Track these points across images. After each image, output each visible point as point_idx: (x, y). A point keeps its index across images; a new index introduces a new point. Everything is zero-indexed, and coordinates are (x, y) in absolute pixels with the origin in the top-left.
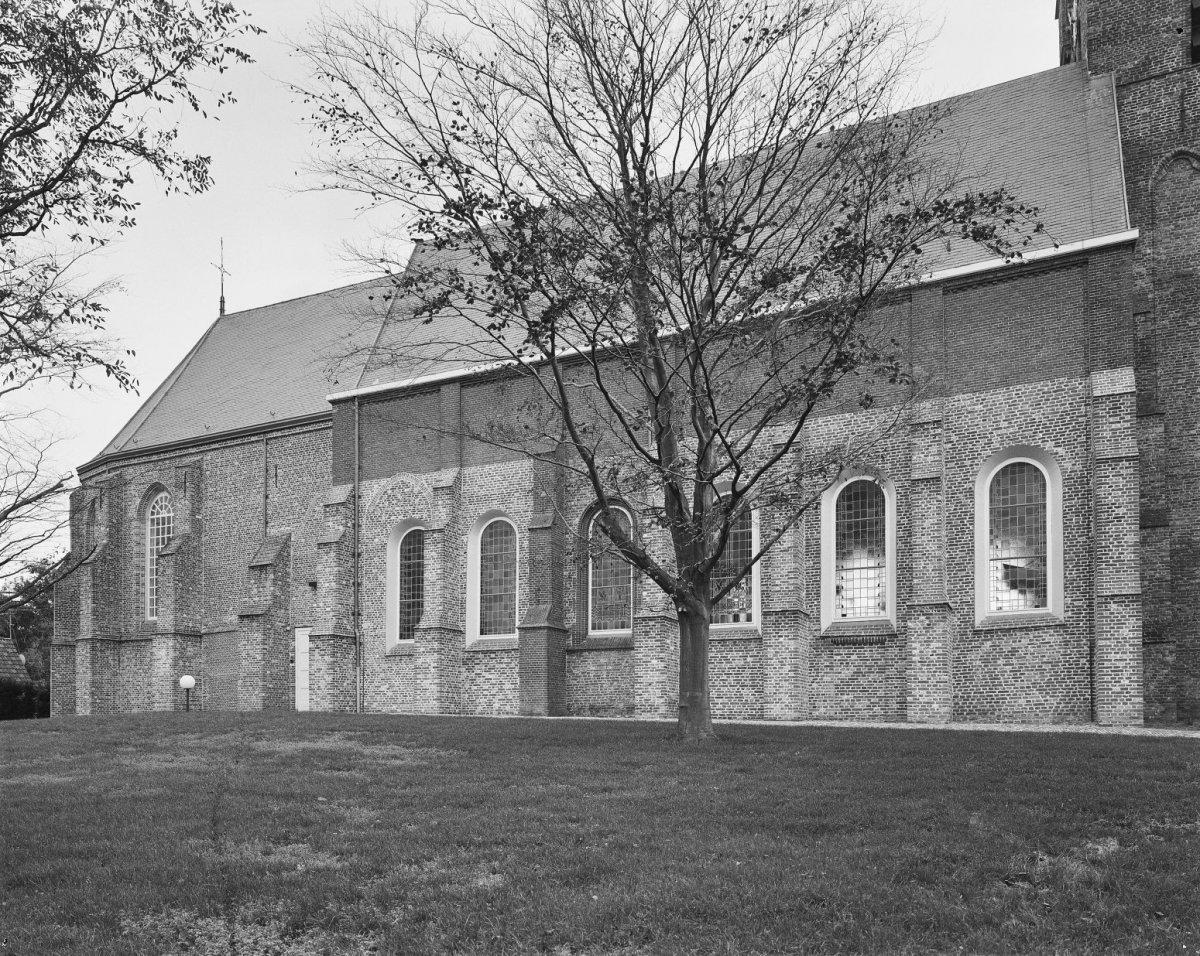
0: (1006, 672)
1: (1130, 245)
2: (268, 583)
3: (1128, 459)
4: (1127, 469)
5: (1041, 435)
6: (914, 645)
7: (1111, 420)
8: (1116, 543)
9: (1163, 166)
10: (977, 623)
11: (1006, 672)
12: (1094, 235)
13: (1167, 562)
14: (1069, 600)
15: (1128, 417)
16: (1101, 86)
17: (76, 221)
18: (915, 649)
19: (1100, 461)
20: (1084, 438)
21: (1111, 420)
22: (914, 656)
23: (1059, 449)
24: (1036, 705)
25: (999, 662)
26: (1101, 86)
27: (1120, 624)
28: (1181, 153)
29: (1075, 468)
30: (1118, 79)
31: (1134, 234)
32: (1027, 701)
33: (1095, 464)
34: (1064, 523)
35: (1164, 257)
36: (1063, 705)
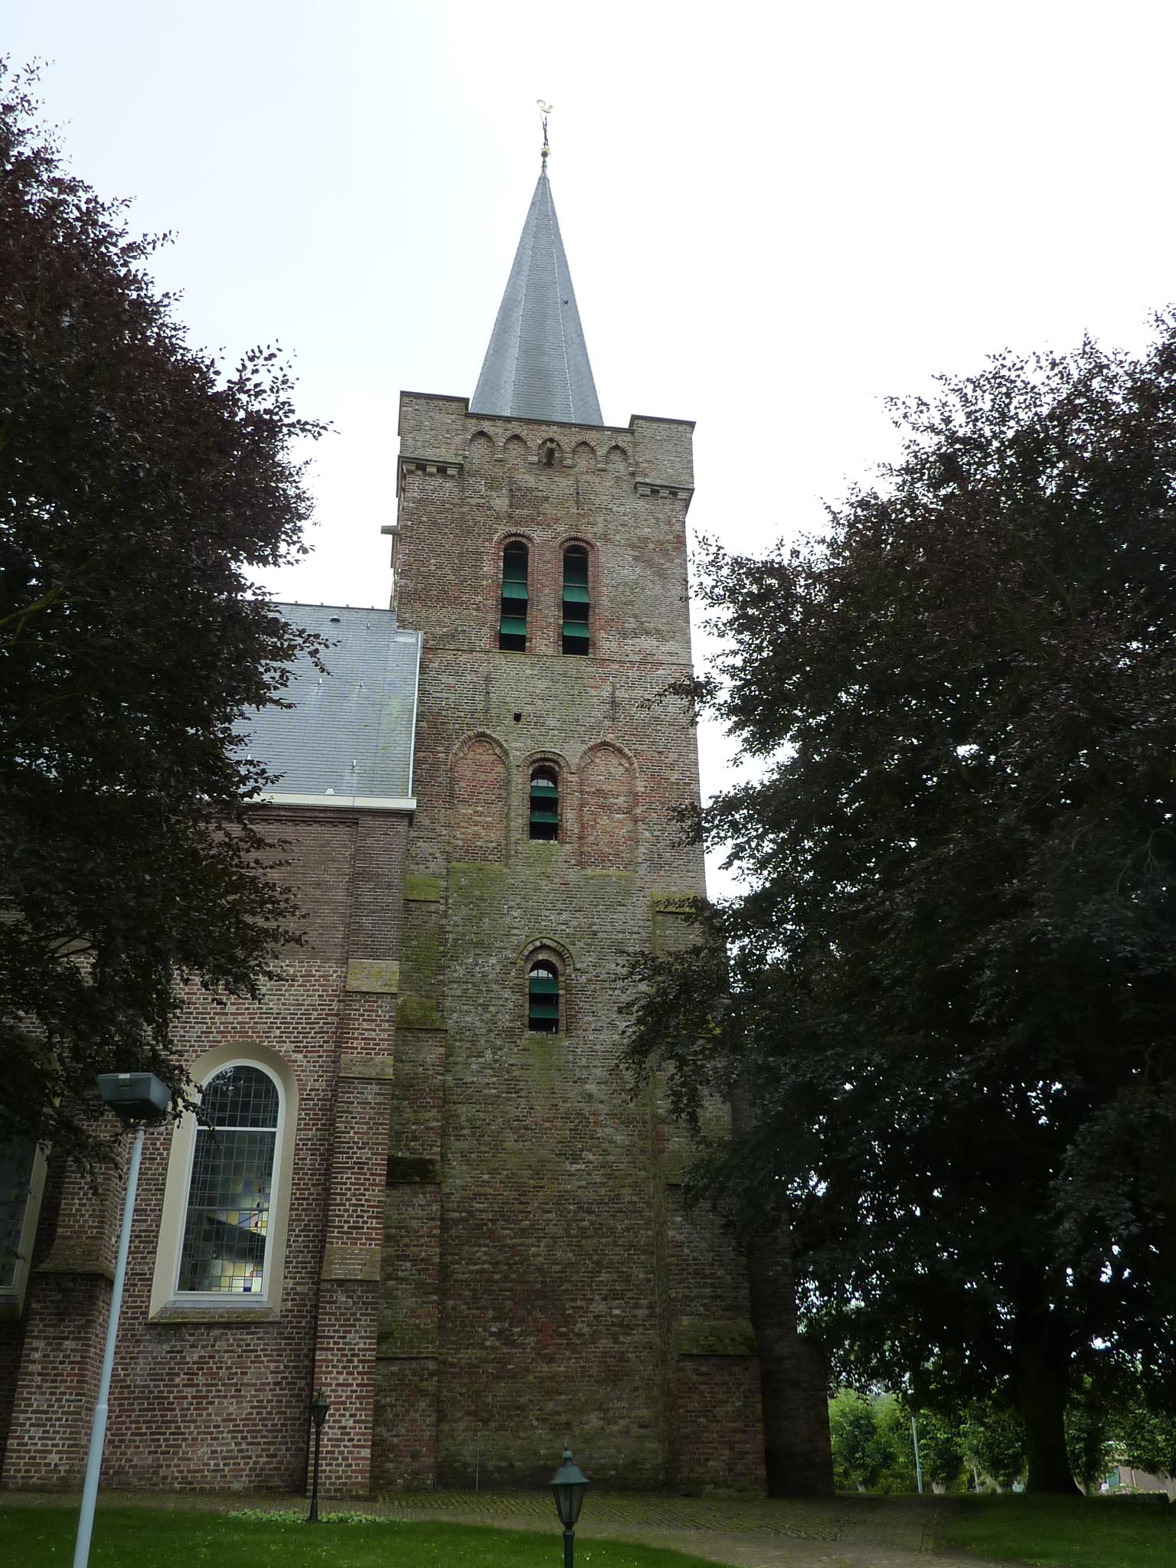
0: (186, 1397)
1: (408, 816)
2: (145, 1027)
3: (380, 1081)
4: (371, 1092)
5: (278, 1031)
6: (36, 1343)
7: (365, 1025)
8: (354, 1202)
9: (464, 742)
10: (154, 1311)
11: (186, 1397)
12: (372, 794)
13: (434, 1236)
14: (290, 1283)
15: (386, 1025)
16: (411, 640)
17: (910, 427)
18: (36, 1350)
19: (349, 1080)
20: (331, 1046)
21: (365, 1025)
22: (34, 1362)
23: (300, 1056)
24: (223, 1458)
25: (177, 1380)
26: (411, 640)
27: (348, 1327)
28: (483, 734)
29: (317, 1085)
30: (426, 641)
31: (410, 804)
32: (213, 1452)
33: (339, 1083)
34: (295, 1164)
35: (460, 843)
36: (265, 1459)
